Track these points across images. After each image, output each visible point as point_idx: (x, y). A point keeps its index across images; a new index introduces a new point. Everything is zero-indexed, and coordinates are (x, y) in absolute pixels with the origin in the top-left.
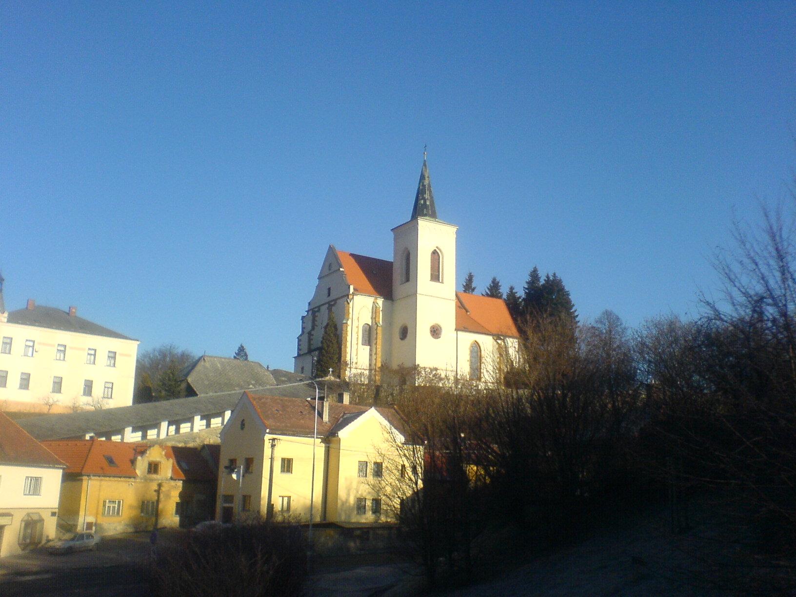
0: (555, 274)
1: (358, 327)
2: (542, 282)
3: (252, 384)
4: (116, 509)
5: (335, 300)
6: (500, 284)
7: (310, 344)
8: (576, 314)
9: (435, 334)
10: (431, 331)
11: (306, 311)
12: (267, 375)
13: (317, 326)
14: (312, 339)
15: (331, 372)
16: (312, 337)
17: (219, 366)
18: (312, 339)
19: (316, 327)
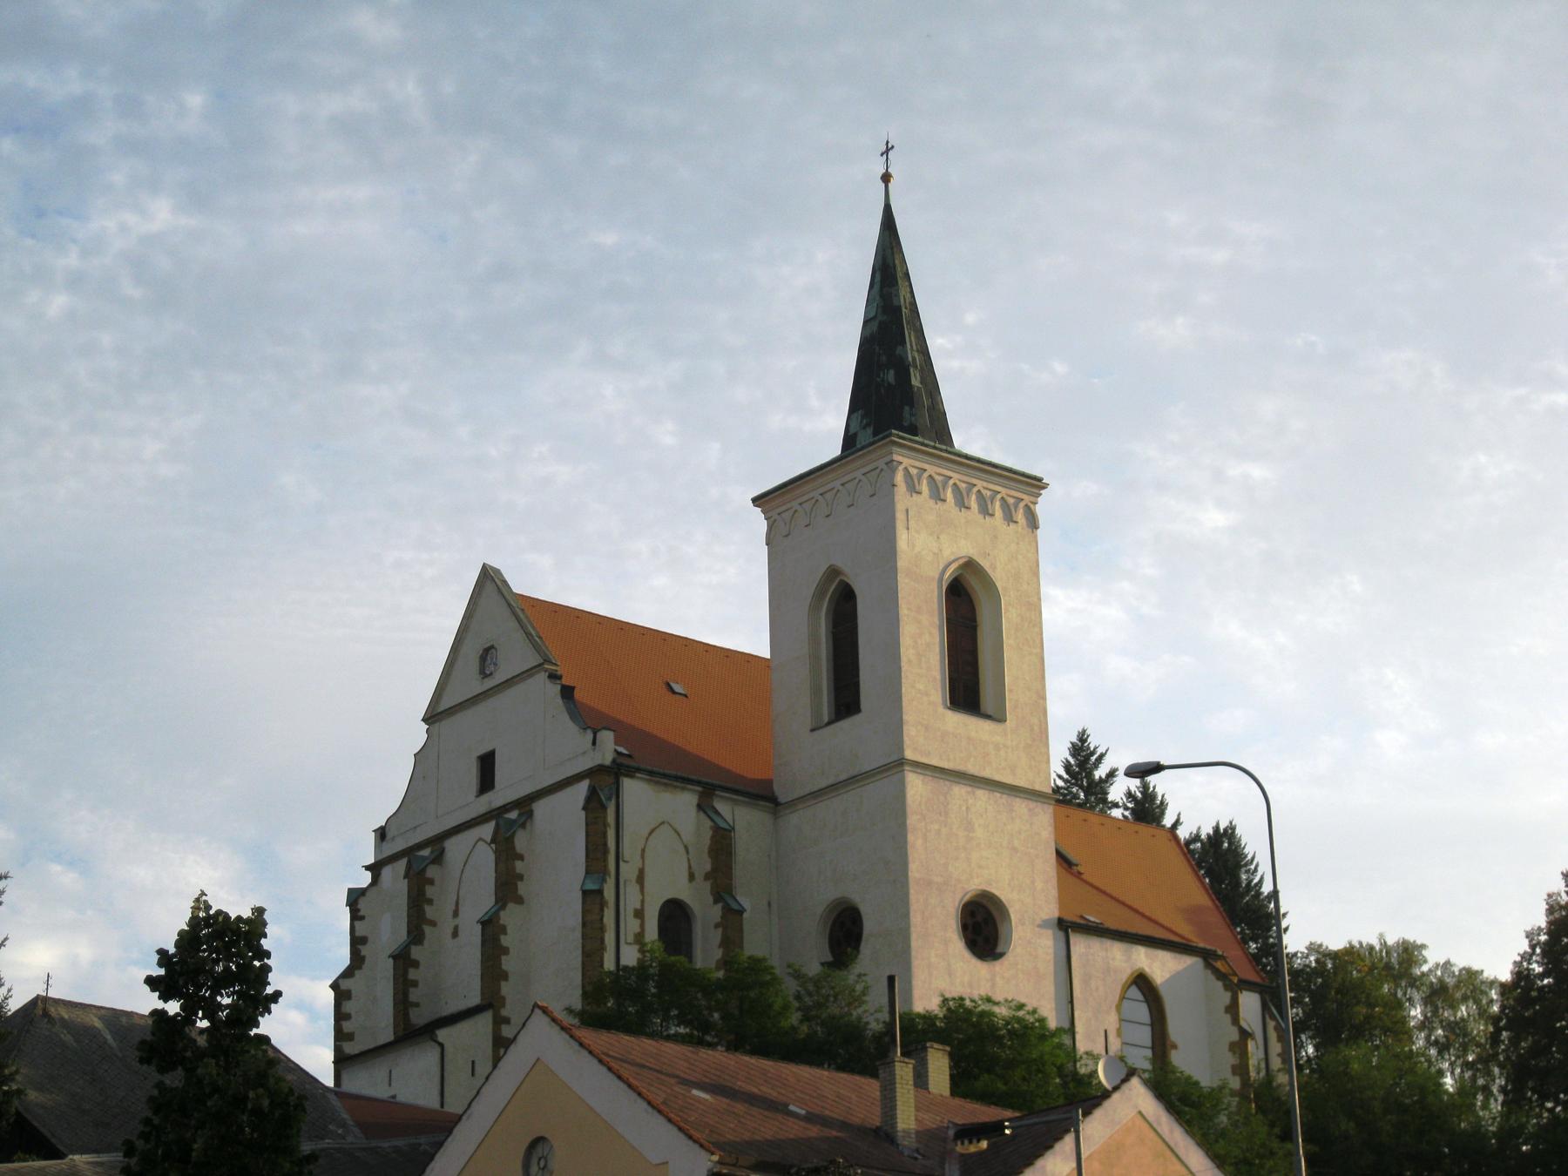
1: (639, 914)
5: (525, 805)
7: (403, 1003)
11: (368, 868)
13: (433, 924)
14: (415, 984)
16: (413, 974)
18: (415, 984)
19: (427, 929)
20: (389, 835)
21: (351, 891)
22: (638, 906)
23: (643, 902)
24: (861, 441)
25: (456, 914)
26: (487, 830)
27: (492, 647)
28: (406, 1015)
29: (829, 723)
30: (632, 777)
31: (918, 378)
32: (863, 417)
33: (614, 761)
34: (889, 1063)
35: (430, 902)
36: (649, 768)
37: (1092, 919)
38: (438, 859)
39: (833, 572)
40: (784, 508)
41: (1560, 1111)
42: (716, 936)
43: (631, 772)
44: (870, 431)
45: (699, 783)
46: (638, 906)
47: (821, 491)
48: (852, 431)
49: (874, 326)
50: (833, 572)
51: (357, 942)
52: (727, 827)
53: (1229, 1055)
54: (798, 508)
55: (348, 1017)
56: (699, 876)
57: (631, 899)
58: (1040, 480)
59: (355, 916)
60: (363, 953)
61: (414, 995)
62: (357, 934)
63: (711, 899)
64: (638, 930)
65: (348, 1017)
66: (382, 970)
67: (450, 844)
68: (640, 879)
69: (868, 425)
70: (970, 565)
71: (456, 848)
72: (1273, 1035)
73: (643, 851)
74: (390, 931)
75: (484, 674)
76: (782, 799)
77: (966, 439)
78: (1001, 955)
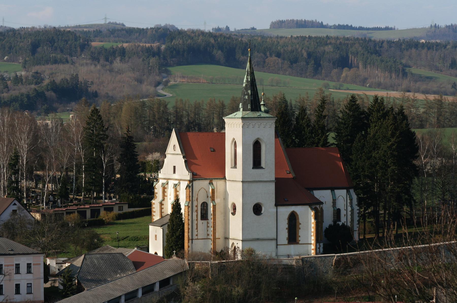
1: (197, 206)
15: (174, 254)
19: (165, 197)
23: (197, 204)
34: (152, 47)
41: (381, 211)
45: (209, 179)
61: (163, 211)
64: (196, 209)
68: (197, 200)
72: (348, 198)
73: (198, 194)
78: (96, 92)
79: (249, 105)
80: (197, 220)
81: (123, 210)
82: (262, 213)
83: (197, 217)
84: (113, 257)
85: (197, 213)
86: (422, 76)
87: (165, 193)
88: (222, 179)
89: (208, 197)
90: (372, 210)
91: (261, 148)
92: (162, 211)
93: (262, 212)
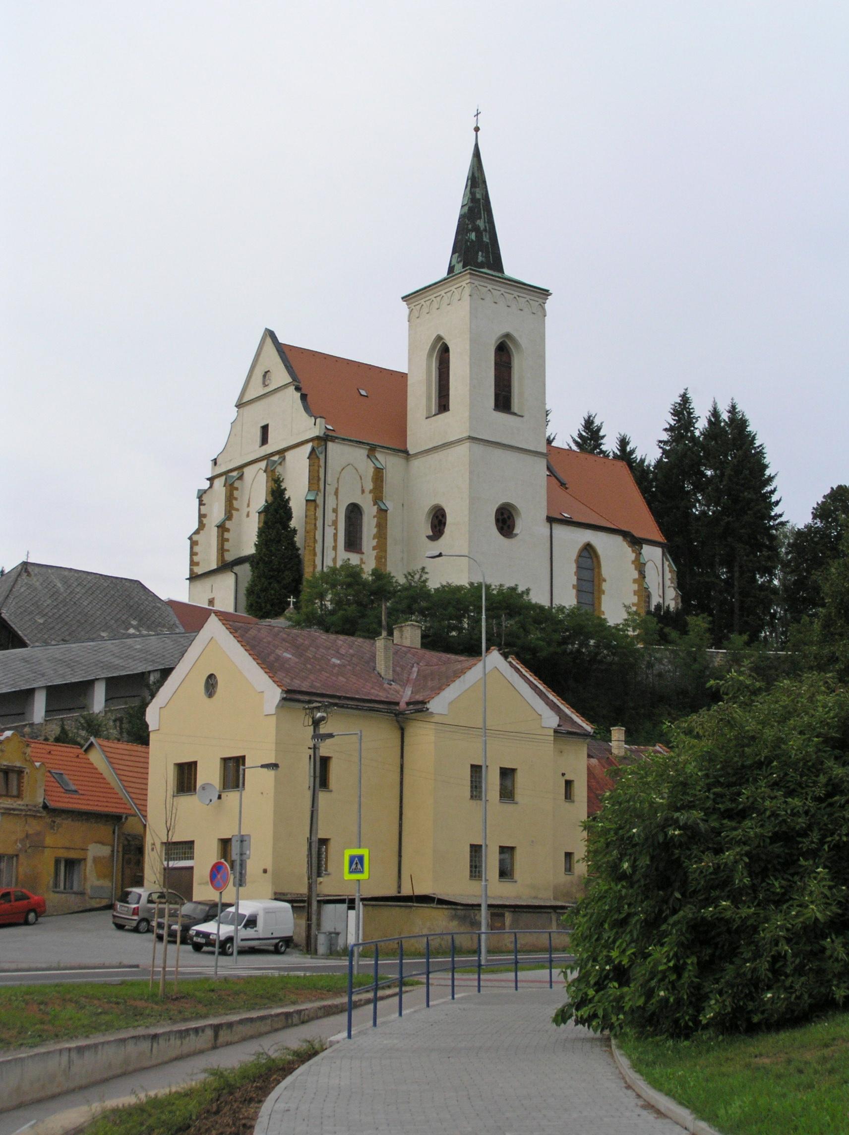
0: (734, 407)
1: (335, 511)
2: (701, 425)
3: (133, 626)
4: (495, 911)
5: (282, 452)
6: (601, 433)
7: (222, 550)
8: (774, 498)
9: (505, 528)
10: (497, 521)
11: (208, 479)
12: (159, 608)
13: (237, 510)
14: (227, 540)
15: (292, 606)
16: (226, 535)
17: (59, 585)
18: (227, 540)
19: (234, 512)
20: (218, 462)
21: (199, 490)
22: (335, 507)
24: (457, 271)
25: (248, 506)
26: (263, 464)
27: (269, 371)
28: (223, 556)
29: (435, 415)
30: (333, 442)
31: (488, 236)
32: (458, 257)
33: (324, 434)
35: (236, 499)
36: (343, 437)
37: (566, 515)
38: (241, 477)
39: (439, 338)
40: (417, 303)
42: (374, 521)
43: (333, 439)
44: (461, 264)
45: (368, 444)
46: (335, 507)
47: (435, 295)
48: (452, 264)
49: (466, 209)
50: (439, 338)
51: (201, 516)
52: (382, 467)
53: (498, 584)
54: (424, 303)
55: (196, 554)
56: (367, 490)
57: (331, 502)
58: (547, 291)
59: (201, 503)
60: (204, 522)
61: (227, 546)
62: (202, 513)
63: (372, 503)
64: (334, 518)
65: (196, 554)
66: (211, 537)
67: (246, 470)
68: (336, 493)
69: (460, 261)
70: (508, 336)
71: (249, 472)
73: (338, 479)
74: (217, 513)
75: (265, 385)
76: (411, 452)
77: (510, 269)
79: (480, 253)
80: (335, 548)
81: (19, 796)
82: (516, 535)
83: (335, 540)
84: (112, 586)
85: (336, 529)
86: (66, 1038)
87: (235, 502)
88: (394, 450)
89: (363, 491)
90: (706, 614)
91: (510, 364)
92: (226, 547)
93: (515, 532)
